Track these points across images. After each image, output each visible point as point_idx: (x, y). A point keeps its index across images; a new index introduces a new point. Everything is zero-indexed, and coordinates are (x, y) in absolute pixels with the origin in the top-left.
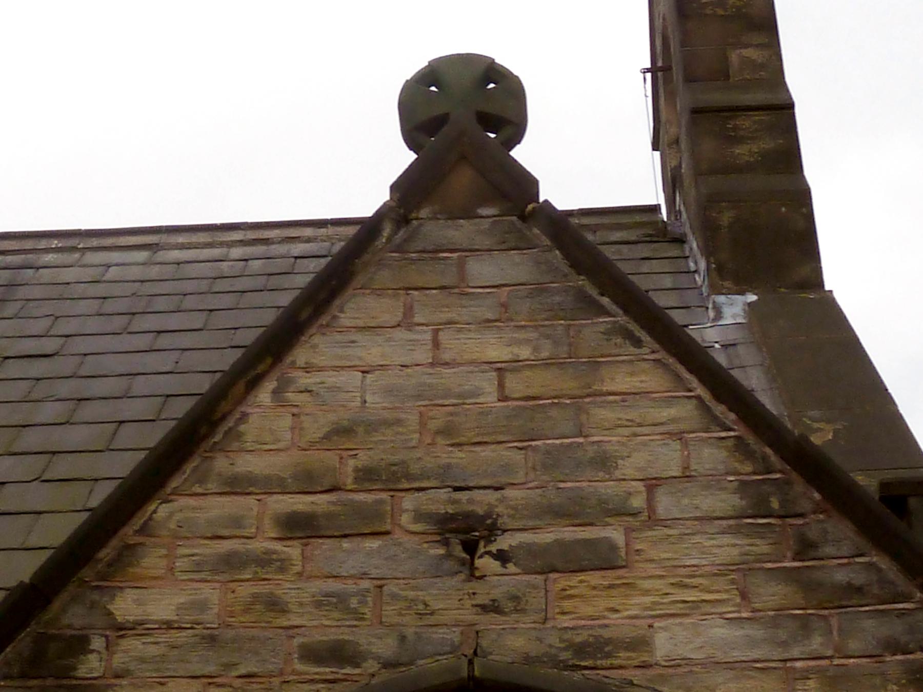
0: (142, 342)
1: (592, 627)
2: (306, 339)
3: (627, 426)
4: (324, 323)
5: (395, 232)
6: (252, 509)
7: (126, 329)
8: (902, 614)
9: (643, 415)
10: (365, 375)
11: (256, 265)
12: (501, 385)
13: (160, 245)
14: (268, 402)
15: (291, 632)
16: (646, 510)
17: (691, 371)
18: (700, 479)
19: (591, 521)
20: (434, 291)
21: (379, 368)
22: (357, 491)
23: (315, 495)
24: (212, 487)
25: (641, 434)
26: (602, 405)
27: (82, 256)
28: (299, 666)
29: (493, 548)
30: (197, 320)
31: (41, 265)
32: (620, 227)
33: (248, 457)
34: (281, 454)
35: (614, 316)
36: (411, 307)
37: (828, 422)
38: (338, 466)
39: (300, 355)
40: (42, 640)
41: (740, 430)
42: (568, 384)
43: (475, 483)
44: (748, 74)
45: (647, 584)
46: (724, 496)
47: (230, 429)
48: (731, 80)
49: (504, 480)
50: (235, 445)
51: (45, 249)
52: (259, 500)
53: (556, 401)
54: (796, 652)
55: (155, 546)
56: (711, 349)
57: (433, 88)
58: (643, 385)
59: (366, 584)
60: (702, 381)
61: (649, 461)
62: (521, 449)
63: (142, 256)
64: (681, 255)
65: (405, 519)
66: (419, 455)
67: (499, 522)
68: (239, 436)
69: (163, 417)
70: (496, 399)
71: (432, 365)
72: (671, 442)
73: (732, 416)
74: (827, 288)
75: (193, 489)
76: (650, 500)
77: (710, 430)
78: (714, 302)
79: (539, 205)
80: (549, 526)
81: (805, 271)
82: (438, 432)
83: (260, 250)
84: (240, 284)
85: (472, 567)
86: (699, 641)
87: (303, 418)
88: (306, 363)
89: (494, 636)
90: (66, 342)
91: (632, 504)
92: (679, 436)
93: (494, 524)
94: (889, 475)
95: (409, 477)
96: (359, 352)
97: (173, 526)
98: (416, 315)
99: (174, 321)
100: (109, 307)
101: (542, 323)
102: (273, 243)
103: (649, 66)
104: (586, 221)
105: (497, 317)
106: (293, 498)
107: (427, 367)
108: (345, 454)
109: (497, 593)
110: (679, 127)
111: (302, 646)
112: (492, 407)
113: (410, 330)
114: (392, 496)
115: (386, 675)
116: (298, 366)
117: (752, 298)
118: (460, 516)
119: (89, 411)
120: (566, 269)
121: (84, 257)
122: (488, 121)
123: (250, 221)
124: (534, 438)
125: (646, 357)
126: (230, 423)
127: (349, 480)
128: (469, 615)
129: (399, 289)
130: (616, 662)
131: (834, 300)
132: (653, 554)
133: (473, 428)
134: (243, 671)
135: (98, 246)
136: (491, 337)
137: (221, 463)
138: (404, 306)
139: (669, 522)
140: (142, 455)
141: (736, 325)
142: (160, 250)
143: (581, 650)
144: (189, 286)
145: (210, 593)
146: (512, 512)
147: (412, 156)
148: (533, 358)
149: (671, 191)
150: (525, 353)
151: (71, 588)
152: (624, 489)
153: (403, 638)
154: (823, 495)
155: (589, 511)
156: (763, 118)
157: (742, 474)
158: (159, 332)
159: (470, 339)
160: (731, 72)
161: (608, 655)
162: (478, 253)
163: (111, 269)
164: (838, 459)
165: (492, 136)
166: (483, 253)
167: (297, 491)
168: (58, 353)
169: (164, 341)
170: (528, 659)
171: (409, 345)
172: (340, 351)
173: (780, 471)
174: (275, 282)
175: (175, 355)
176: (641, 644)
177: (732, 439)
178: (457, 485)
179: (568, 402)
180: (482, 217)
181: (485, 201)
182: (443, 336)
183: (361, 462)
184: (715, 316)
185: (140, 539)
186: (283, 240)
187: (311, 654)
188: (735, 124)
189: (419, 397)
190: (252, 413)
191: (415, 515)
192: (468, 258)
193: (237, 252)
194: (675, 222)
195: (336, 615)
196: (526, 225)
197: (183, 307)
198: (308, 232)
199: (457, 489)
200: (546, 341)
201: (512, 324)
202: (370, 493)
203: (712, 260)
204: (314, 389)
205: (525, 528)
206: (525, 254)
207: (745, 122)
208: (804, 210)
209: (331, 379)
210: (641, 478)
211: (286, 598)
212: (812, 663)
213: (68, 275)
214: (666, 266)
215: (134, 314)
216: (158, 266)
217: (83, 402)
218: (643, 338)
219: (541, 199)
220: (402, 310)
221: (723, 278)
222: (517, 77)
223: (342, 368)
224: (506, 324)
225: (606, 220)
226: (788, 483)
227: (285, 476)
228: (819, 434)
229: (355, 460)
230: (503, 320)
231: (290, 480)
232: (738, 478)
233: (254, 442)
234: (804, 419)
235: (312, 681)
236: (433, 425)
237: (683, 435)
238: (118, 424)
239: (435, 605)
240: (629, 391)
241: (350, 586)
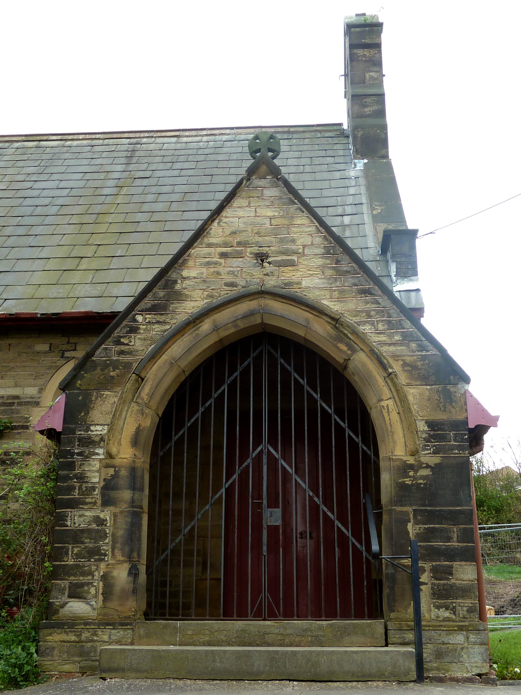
0: (176, 173)
1: (289, 279)
5: (246, 183)
7: (171, 168)
8: (357, 277)
12: (271, 222)
15: (222, 280)
24: (204, 246)
26: (294, 227)
28: (224, 287)
29: (268, 261)
30: (193, 165)
32: (330, 131)
33: (212, 238)
37: (380, 206)
39: (224, 214)
40: (167, 281)
42: (286, 222)
45: (301, 270)
46: (320, 249)
50: (209, 236)
54: (333, 286)
55: (192, 259)
59: (238, 269)
63: (174, 140)
71: (255, 216)
73: (324, 230)
82: (256, 233)
83: (212, 138)
84: (207, 151)
85: (263, 266)
86: (312, 283)
89: (267, 281)
92: (311, 235)
95: (249, 244)
96: (238, 213)
97: (195, 255)
99: (186, 165)
100: (166, 159)
102: (217, 135)
109: (268, 271)
111: (224, 283)
115: (243, 289)
117: (366, 161)
119: (162, 198)
120: (287, 193)
126: (208, 230)
128: (261, 276)
130: (293, 287)
131: (391, 163)
132: (303, 263)
134: (211, 288)
136: (269, 210)
137: (206, 240)
143: (286, 284)
144: (190, 152)
145: (204, 270)
150: (276, 214)
151: (173, 269)
153: (247, 281)
158: (182, 169)
161: (292, 286)
169: (184, 173)
170: (274, 286)
172: (233, 213)
175: (187, 178)
176: (299, 283)
185: (188, 258)
187: (227, 284)
189: (251, 225)
195: (232, 276)
197: (189, 160)
198: (228, 131)
199: (260, 247)
207: (368, 100)
208: (385, 131)
209: (231, 220)
211: (221, 272)
212: (337, 288)
213: (152, 147)
226: (335, 247)
235: (227, 291)
236: (255, 232)
239: (254, 274)
241: (235, 269)
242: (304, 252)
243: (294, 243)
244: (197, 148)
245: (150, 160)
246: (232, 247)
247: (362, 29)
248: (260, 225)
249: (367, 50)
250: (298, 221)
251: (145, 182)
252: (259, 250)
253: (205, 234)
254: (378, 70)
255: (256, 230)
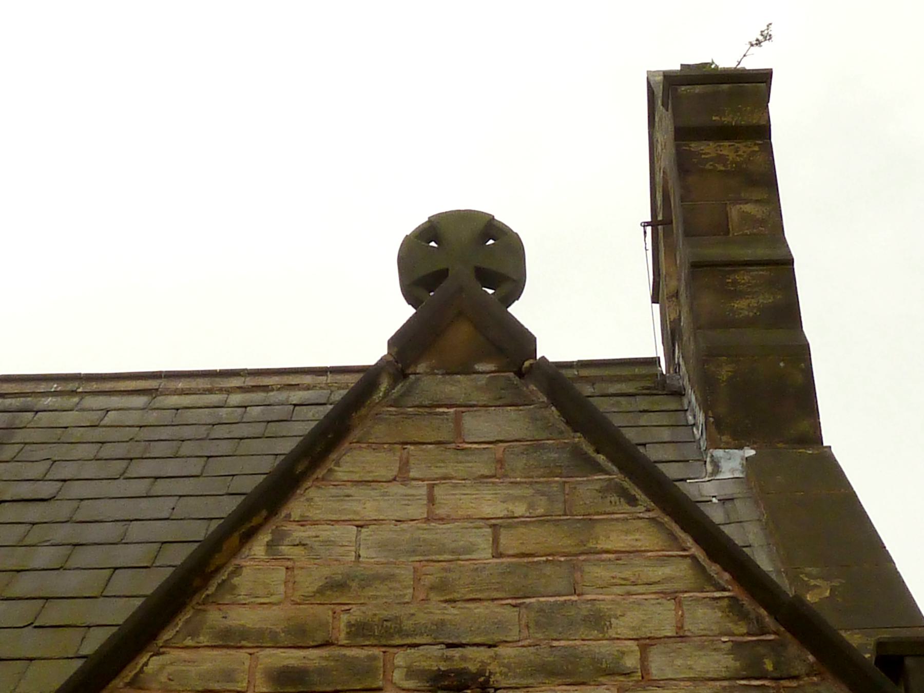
0: (140, 487)
2: (302, 492)
3: (621, 585)
4: (320, 476)
5: (393, 386)
6: (244, 663)
9: (637, 573)
10: (359, 529)
11: (255, 412)
12: (496, 541)
13: (160, 390)
14: (262, 555)
16: (639, 670)
17: (684, 529)
18: (695, 639)
19: (585, 681)
20: (430, 446)
21: (375, 522)
22: (351, 646)
23: (308, 650)
24: (204, 640)
25: (634, 593)
27: (81, 400)
30: (194, 467)
31: (42, 408)
33: (242, 610)
34: (275, 607)
35: (610, 474)
36: (407, 462)
38: (331, 621)
39: (296, 508)
41: (734, 591)
42: (566, 543)
43: (468, 640)
44: (747, 229)
46: (716, 656)
47: (224, 581)
48: (731, 235)
49: (497, 638)
50: (228, 598)
51: (44, 392)
52: (250, 654)
53: (550, 558)
56: (709, 503)
57: (433, 244)
58: (639, 544)
60: (697, 540)
61: (643, 620)
62: (514, 606)
63: (140, 401)
64: (679, 408)
65: (397, 676)
66: (412, 611)
67: (491, 680)
68: (234, 587)
69: (158, 564)
70: (490, 556)
71: (427, 520)
72: (664, 601)
73: (727, 576)
74: (825, 444)
75: (184, 642)
76: (643, 659)
77: (705, 590)
78: (712, 456)
79: (535, 362)
80: (542, 685)
81: (804, 426)
82: (432, 588)
84: (238, 431)
87: (296, 572)
88: (301, 516)
90: (62, 486)
91: (625, 663)
92: (673, 596)
93: (487, 681)
94: (885, 635)
96: (356, 506)
97: (163, 678)
98: (413, 470)
99: (171, 467)
100: (107, 451)
101: (538, 480)
102: (272, 390)
103: (649, 219)
104: (585, 372)
105: (493, 472)
106: (284, 652)
107: (421, 523)
108: (338, 608)
110: (679, 280)
112: (485, 563)
113: (405, 485)
114: (384, 652)
116: (292, 519)
118: (452, 673)
119: (83, 557)
120: (562, 426)
121: (83, 400)
122: (486, 277)
123: (249, 367)
124: (527, 595)
125: (641, 515)
127: (343, 635)
129: (395, 443)
133: (467, 585)
135: (97, 390)
136: (487, 493)
137: (214, 617)
138: (401, 461)
139: (661, 682)
140: (138, 602)
141: (734, 480)
142: (159, 396)
144: (186, 432)
146: (505, 670)
147: (410, 311)
148: (528, 514)
149: (670, 343)
150: (520, 509)
152: (617, 648)
154: (817, 659)
155: (581, 669)
156: (761, 273)
157: (737, 635)
158: (157, 478)
159: (467, 494)
160: (730, 227)
162: (475, 409)
163: (109, 413)
164: (831, 618)
165: (490, 291)
166: (479, 408)
167: (290, 645)
168: (55, 497)
169: (161, 487)
171: (405, 500)
172: (336, 505)
173: (775, 633)
174: (273, 428)
175: (171, 502)
177: (726, 599)
178: (450, 642)
179: (562, 559)
180: (479, 373)
181: (481, 359)
182: (437, 490)
183: (355, 617)
184: (713, 470)
186: (282, 388)
188: (735, 278)
189: (414, 552)
190: (245, 566)
191: (407, 671)
192: (464, 414)
193: (236, 399)
194: (674, 375)
196: (523, 381)
197: (181, 453)
198: (308, 380)
199: (450, 646)
200: (541, 497)
201: (508, 480)
202: (362, 649)
203: (710, 413)
204: (308, 542)
205: (518, 686)
206: (521, 410)
207: (744, 277)
209: (326, 532)
210: (634, 637)
214: (664, 419)
215: (131, 459)
216: (156, 411)
217: (77, 547)
218: (638, 497)
219: (538, 356)
220: (398, 465)
221: (721, 433)
222: (516, 234)
223: (337, 521)
224: (501, 480)
225: (606, 372)
227: (278, 630)
228: (816, 591)
229: (348, 615)
230: (498, 476)
231: (283, 635)
232: (732, 638)
233: (246, 595)
234: (801, 576)
236: (428, 581)
237: (677, 594)
238: (152, 480)
240: (624, 549)
242: (645, 670)
243: (603, 632)
244: (209, 421)
245: (57, 452)
246: (326, 644)
247: (709, 88)
248: (453, 552)
249: (726, 143)
250: (613, 536)
251: (34, 512)
252: (447, 659)
253: (209, 592)
254: (765, 196)
255: (431, 578)
